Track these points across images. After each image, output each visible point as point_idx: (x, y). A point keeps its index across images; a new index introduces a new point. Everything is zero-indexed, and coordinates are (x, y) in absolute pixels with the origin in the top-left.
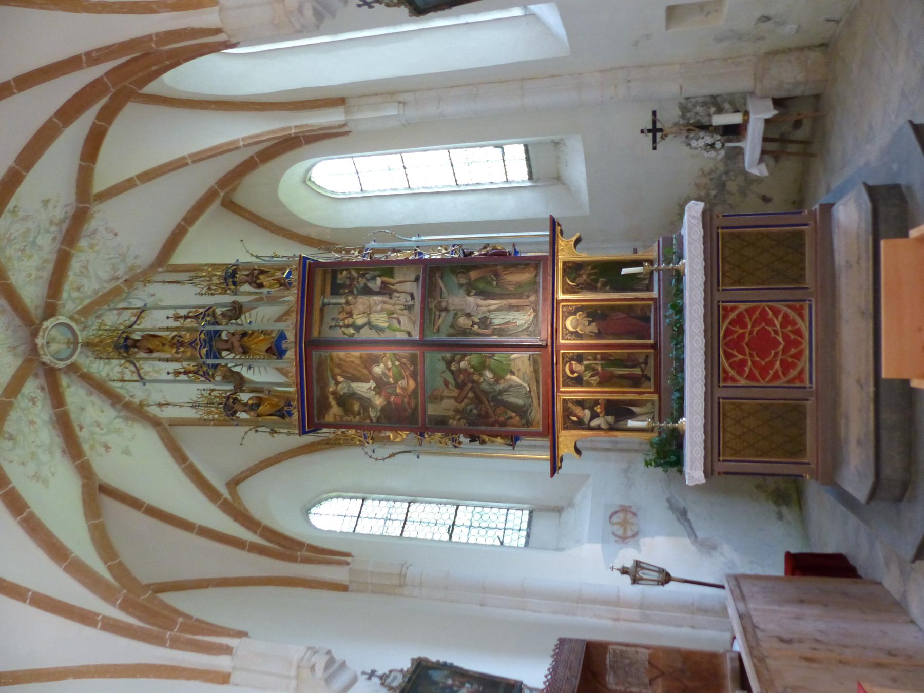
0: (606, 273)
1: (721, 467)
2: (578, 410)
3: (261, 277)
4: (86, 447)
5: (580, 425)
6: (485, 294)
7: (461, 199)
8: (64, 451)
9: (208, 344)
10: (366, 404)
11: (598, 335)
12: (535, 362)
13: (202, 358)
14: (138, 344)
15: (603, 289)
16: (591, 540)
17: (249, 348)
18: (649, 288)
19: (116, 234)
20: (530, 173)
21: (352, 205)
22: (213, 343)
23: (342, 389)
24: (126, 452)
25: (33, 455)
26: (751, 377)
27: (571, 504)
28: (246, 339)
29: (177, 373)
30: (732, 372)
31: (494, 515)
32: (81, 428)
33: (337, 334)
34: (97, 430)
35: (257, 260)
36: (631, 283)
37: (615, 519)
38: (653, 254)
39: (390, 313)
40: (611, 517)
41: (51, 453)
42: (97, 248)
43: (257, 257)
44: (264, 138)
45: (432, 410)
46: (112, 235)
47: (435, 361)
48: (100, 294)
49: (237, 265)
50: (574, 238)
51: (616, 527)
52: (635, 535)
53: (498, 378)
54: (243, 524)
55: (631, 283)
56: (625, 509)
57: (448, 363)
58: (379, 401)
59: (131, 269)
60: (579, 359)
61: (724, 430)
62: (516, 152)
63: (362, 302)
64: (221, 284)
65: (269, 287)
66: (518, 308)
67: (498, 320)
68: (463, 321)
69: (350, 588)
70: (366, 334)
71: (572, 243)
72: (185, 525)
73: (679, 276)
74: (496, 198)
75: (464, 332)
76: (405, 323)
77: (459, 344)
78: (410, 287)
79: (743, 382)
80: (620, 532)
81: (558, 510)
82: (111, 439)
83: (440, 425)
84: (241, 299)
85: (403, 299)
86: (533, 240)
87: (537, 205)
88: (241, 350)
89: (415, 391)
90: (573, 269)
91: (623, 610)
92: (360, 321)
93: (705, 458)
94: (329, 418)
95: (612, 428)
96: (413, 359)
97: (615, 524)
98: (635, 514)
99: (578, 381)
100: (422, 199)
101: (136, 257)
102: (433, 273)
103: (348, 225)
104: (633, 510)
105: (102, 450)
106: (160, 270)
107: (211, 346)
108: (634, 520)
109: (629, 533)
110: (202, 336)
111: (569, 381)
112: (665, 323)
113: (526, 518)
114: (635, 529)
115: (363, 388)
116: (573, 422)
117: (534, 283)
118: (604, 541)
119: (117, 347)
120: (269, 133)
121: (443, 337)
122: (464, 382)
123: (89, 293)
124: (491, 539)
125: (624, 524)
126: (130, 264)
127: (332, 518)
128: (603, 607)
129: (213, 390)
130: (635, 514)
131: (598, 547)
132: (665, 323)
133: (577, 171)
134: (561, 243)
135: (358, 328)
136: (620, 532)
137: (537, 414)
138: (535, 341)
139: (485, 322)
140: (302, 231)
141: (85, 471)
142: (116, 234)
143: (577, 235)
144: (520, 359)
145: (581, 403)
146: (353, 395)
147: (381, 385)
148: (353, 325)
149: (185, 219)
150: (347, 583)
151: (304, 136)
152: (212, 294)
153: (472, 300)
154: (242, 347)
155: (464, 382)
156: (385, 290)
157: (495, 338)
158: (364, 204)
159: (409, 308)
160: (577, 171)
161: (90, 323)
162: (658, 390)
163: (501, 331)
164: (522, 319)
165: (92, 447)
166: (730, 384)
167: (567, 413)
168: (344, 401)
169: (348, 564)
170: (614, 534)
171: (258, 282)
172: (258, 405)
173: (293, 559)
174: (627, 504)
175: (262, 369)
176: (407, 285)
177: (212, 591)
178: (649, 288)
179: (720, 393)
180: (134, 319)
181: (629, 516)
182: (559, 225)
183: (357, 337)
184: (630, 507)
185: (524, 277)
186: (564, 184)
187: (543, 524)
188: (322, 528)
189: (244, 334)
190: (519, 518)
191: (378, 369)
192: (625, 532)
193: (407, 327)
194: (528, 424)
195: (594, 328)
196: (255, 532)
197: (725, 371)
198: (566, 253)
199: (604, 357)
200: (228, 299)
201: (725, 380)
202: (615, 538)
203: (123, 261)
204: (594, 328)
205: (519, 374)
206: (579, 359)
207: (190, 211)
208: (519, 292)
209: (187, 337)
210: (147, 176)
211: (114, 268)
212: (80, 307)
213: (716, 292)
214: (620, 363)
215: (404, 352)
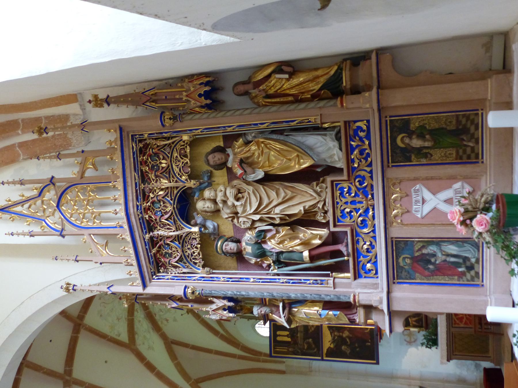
4: (160, 323)
8: (153, 329)
24: (175, 320)
25: (145, 337)
26: (466, 323)
30: (457, 322)
34: (161, 313)
41: (149, 332)
61: (455, 337)
79: (462, 325)
80: (408, 339)
91: (412, 381)
93: (447, 355)
105: (165, 322)
109: (413, 340)
128: (403, 380)
136: (408, 339)
141: (164, 336)
165: (162, 322)
166: (456, 326)
170: (405, 340)
173: (258, 361)
177: (225, 379)
179: (453, 330)
188: (260, 333)
196: (238, 348)
197: (455, 321)
201: (455, 324)
202: (406, 343)
213: (451, 328)
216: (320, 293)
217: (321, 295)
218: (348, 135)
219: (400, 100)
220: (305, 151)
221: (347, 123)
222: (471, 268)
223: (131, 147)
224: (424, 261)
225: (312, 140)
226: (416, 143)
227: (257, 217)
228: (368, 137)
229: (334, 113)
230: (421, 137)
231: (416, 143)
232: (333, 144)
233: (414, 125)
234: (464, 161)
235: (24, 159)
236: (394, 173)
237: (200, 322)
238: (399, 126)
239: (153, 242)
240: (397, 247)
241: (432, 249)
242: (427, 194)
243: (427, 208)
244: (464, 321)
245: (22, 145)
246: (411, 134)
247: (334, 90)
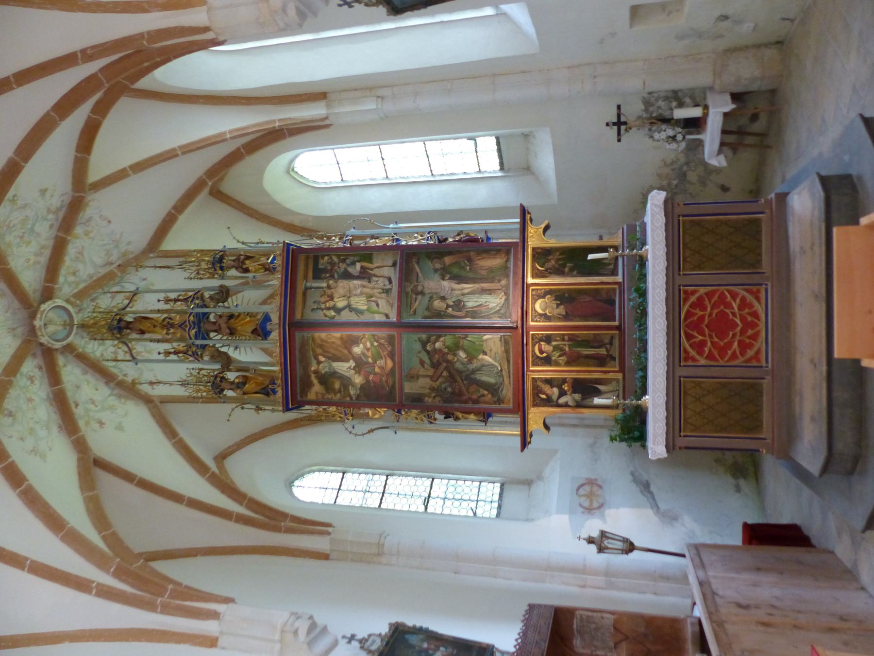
0: (573, 259)
1: (681, 442)
2: (547, 388)
3: (247, 262)
5: (549, 402)
7: (436, 188)
8: (60, 427)
9: (197, 326)
10: (346, 382)
11: (566, 317)
12: (506, 343)
13: (191, 339)
14: (131, 326)
15: (570, 274)
16: (559, 511)
17: (236, 330)
18: (614, 273)
19: (109, 222)
20: (502, 164)
21: (333, 194)
22: (201, 325)
23: (324, 368)
24: (120, 428)
26: (710, 357)
27: (540, 477)
28: (232, 321)
29: (168, 353)
30: (692, 353)
31: (467, 488)
32: (77, 405)
33: (319, 316)
34: (92, 407)
35: (244, 246)
36: (596, 268)
37: (581, 491)
38: (618, 240)
39: (369, 297)
40: (578, 490)
41: (48, 429)
42: (91, 235)
43: (243, 243)
44: (250, 131)
45: (409, 388)
46: (106, 223)
47: (411, 341)
48: (95, 278)
49: (224, 251)
50: (543, 226)
51: (583, 499)
52: (601, 507)
53: (471, 358)
54: (230, 496)
56: (591, 482)
57: (424, 344)
58: (358, 380)
59: (124, 254)
60: (548, 339)
62: (488, 144)
63: (342, 286)
64: (209, 268)
65: (255, 272)
66: (490, 292)
67: (471, 302)
68: (438, 304)
69: (331, 557)
71: (541, 230)
72: (175, 497)
74: (469, 187)
75: (439, 314)
76: (382, 303)
77: (434, 325)
78: (388, 271)
79: (703, 362)
80: (586, 504)
81: (528, 483)
82: (105, 416)
83: (416, 402)
84: (228, 283)
85: (382, 283)
86: (504, 228)
87: (507, 194)
88: (228, 331)
89: (392, 370)
90: (542, 254)
91: (589, 577)
92: (341, 304)
93: (667, 433)
94: (311, 396)
95: (578, 405)
96: (391, 340)
97: (582, 496)
98: (600, 487)
99: (547, 361)
100: (399, 189)
101: (129, 243)
102: (409, 258)
103: (329, 213)
104: (599, 483)
106: (151, 255)
107: (199, 328)
108: (600, 492)
109: (595, 505)
110: (192, 318)
111: (538, 361)
112: (629, 305)
113: (497, 490)
114: (601, 501)
115: (344, 367)
117: (506, 268)
118: (571, 512)
119: (111, 329)
120: (254, 126)
121: (419, 319)
122: (439, 362)
123: (85, 277)
125: (590, 496)
126: (123, 250)
127: (314, 490)
128: (571, 575)
129: (201, 369)
130: (600, 487)
132: (629, 305)
133: (546, 162)
134: (531, 230)
135: (339, 311)
136: (586, 504)
137: (508, 392)
138: (507, 322)
139: (458, 305)
140: (286, 219)
141: (80, 446)
142: (109, 222)
143: (546, 222)
144: (492, 340)
145: (549, 382)
146: (334, 374)
147: (360, 365)
148: (334, 308)
149: (175, 207)
150: (328, 552)
151: (287, 129)
152: (201, 279)
153: (446, 284)
154: (229, 328)
155: (439, 362)
156: (365, 275)
157: (468, 320)
158: (344, 193)
159: (387, 291)
160: (546, 162)
161: (85, 306)
163: (473, 314)
164: (494, 302)
165: (87, 423)
166: (690, 363)
167: (537, 391)
168: (326, 380)
169: (329, 533)
170: (581, 505)
171: (244, 267)
172: (244, 384)
173: (277, 529)
174: (593, 477)
175: (248, 349)
176: (385, 270)
177: (200, 560)
178: (614, 273)
179: (681, 372)
180: (126, 302)
181: (595, 488)
182: (529, 213)
183: (338, 319)
184: (596, 480)
185: (496, 262)
186: (533, 174)
187: (514, 496)
188: (301, 499)
189: (231, 316)
190: (491, 490)
191: (357, 350)
192: (591, 504)
193: (385, 309)
194: (500, 401)
195: (562, 310)
198: (535, 240)
199: (572, 338)
200: (216, 283)
201: (686, 359)
202: (582, 510)
203: (117, 247)
204: (562, 310)
205: (491, 354)
206: (548, 339)
207: (179, 200)
208: (491, 276)
209: (177, 319)
210: (139, 167)
211: (108, 253)
212: (75, 291)
213: (677, 277)
214: (586, 343)
215: (383, 333)
216: (442, 236)
237: (174, 445)
244: (706, 350)
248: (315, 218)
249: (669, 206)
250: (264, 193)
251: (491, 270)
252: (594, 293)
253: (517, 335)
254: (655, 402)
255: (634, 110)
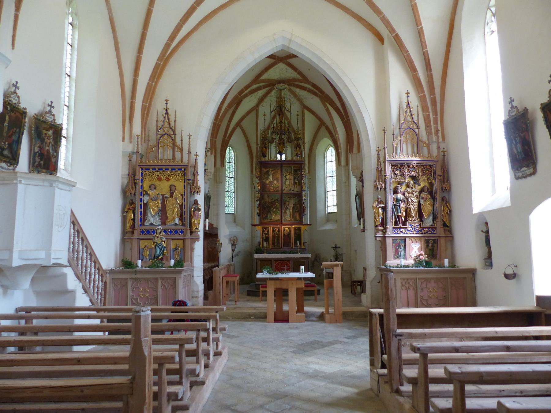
0: (298, 236)
1: (258, 261)
2: (266, 231)
5: (263, 231)
6: (294, 208)
7: (323, 193)
10: (267, 179)
11: (284, 235)
12: (277, 221)
15: (295, 236)
16: (229, 232)
18: (295, 247)
20: (330, 213)
21: (323, 159)
22: (281, 130)
23: (270, 172)
27: (237, 225)
31: (232, 204)
33: (284, 171)
36: (296, 243)
38: (303, 247)
39: (289, 185)
45: (266, 196)
47: (278, 196)
53: (274, 212)
55: (296, 243)
57: (277, 200)
58: (267, 182)
60: (279, 231)
62: (335, 210)
63: (292, 177)
66: (290, 216)
67: (288, 212)
68: (287, 203)
70: (284, 179)
73: (297, 253)
74: (323, 203)
75: (285, 204)
76: (287, 189)
77: (282, 202)
78: (296, 189)
81: (235, 222)
83: (261, 198)
85: (293, 188)
86: (307, 219)
87: (320, 214)
89: (270, 191)
90: (299, 229)
92: (287, 177)
94: (263, 169)
95: (263, 238)
96: (278, 191)
99: (273, 231)
100: (323, 181)
102: (299, 196)
103: (316, 158)
111: (273, 229)
112: (287, 250)
113: (232, 213)
115: (271, 178)
116: (300, 244)
117: (297, 220)
118: (230, 235)
121: (283, 198)
122: (273, 203)
124: (227, 203)
127: (230, 154)
131: (228, 233)
132: (287, 250)
133: (329, 227)
134: (306, 227)
135: (285, 177)
137: (265, 221)
138: (283, 221)
139: (287, 209)
140: (315, 143)
141: (257, 105)
144: (278, 217)
145: (268, 231)
146: (269, 175)
147: (271, 183)
148: (286, 175)
153: (292, 205)
155: (273, 203)
156: (295, 183)
157: (283, 211)
158: (322, 163)
159: (290, 190)
160: (329, 227)
162: (272, 249)
163: (285, 212)
164: (288, 218)
167: (266, 228)
168: (267, 173)
176: (296, 189)
178: (295, 247)
183: (283, 177)
185: (298, 218)
187: (231, 218)
189: (284, 144)
190: (232, 211)
191: (275, 182)
193: (286, 189)
194: (263, 219)
195: (286, 234)
198: (303, 227)
199: (279, 237)
204: (286, 234)
205: (275, 217)
206: (279, 231)
208: (294, 217)
209: (283, 125)
214: (278, 240)
215: (280, 189)
216: (305, 203)
217: (35, 154)
218: (432, 228)
219: (442, 241)
220: (429, 216)
221: (436, 228)
222: (398, 257)
223: (432, 163)
224: (399, 246)
225: (431, 218)
226: (430, 245)
227: (410, 200)
228: (432, 233)
229: (439, 225)
230: (432, 246)
231: (430, 245)
232: (431, 224)
233: (435, 245)
234: (159, 307)
235: (424, 115)
236: (423, 240)
238: (435, 241)
239: (403, 166)
240: (403, 239)
241: (402, 248)
242: (417, 247)
243: (414, 247)
245: (429, 115)
246: (432, 244)
247: (445, 225)
248: (315, 153)
249: (308, 258)
250: (323, 138)
251: (296, 217)
252: (290, 242)
253: (280, 223)
254: (265, 255)
255: (339, 251)
